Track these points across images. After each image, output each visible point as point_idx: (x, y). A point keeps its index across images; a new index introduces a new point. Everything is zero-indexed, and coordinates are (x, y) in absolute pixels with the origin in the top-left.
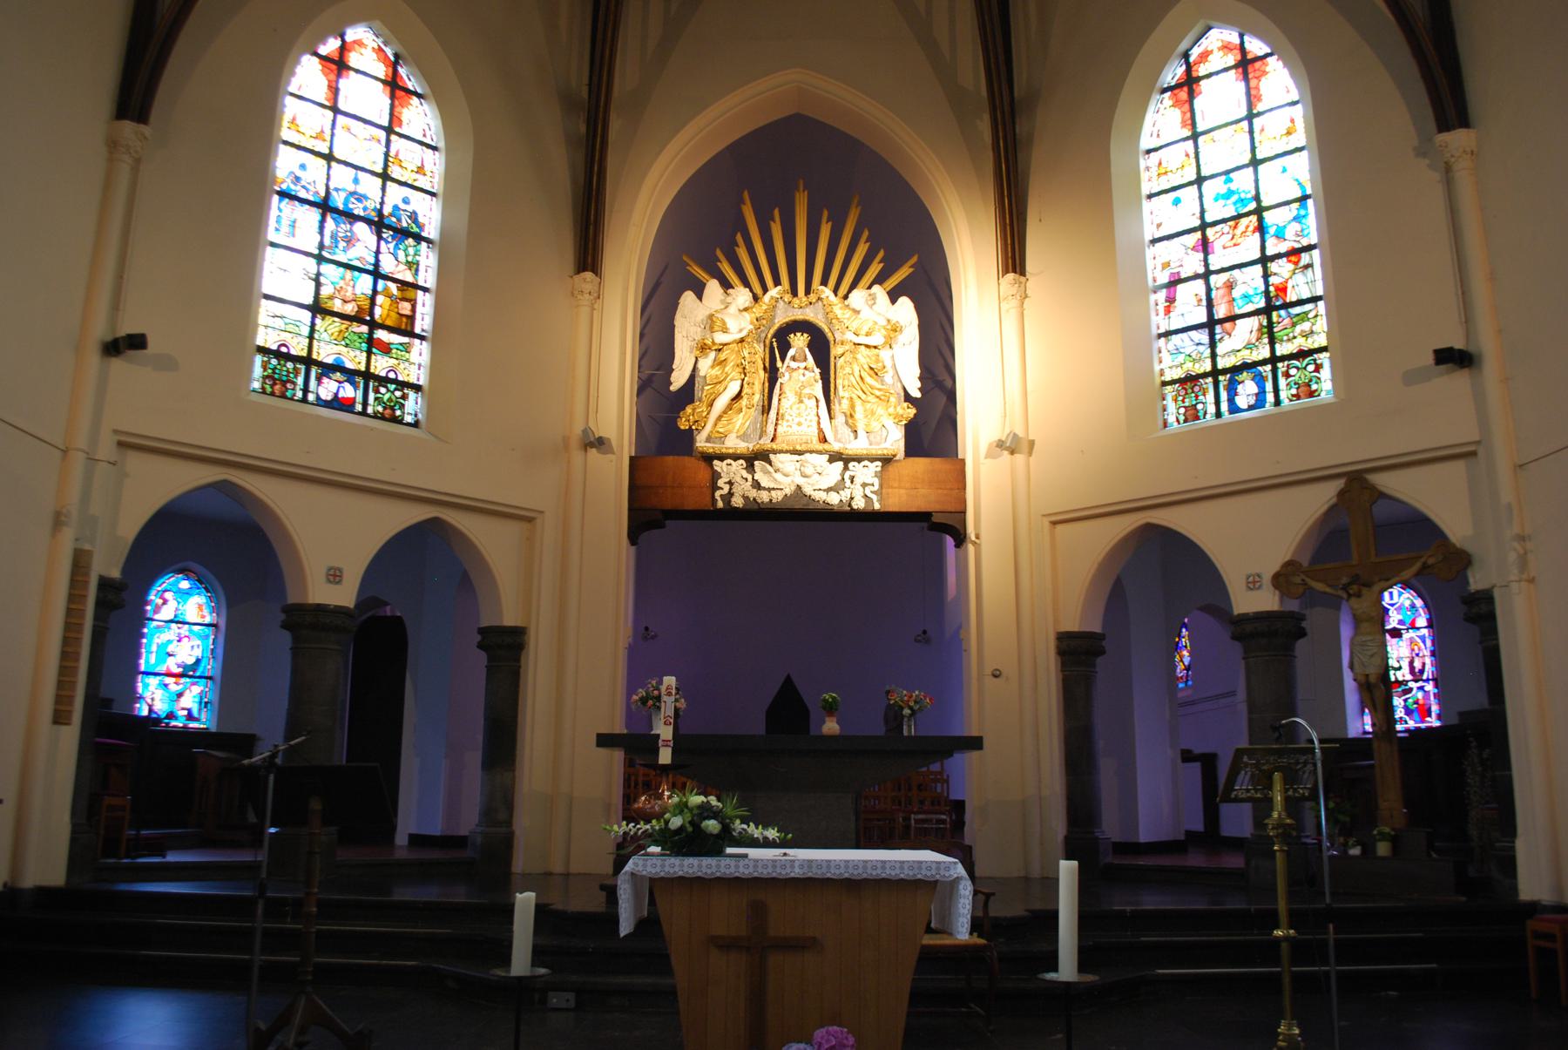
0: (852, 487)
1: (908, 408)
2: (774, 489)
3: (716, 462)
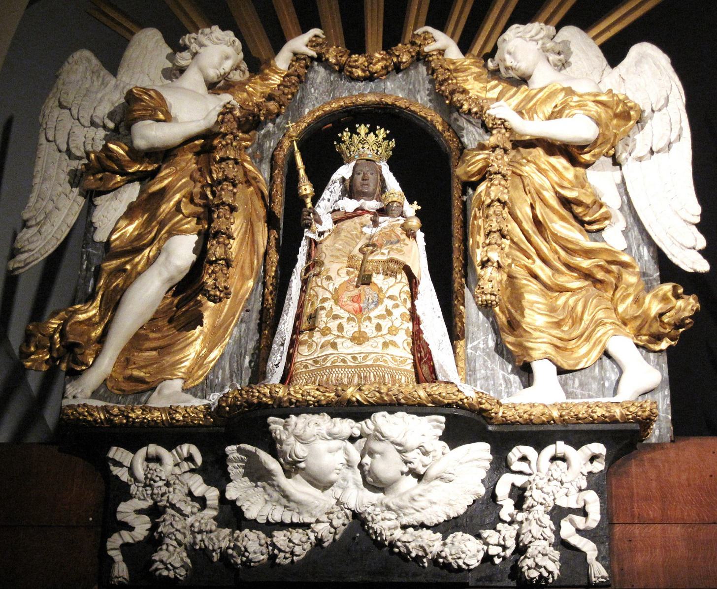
0: (520, 517)
1: (677, 297)
2: (282, 526)
3: (117, 453)
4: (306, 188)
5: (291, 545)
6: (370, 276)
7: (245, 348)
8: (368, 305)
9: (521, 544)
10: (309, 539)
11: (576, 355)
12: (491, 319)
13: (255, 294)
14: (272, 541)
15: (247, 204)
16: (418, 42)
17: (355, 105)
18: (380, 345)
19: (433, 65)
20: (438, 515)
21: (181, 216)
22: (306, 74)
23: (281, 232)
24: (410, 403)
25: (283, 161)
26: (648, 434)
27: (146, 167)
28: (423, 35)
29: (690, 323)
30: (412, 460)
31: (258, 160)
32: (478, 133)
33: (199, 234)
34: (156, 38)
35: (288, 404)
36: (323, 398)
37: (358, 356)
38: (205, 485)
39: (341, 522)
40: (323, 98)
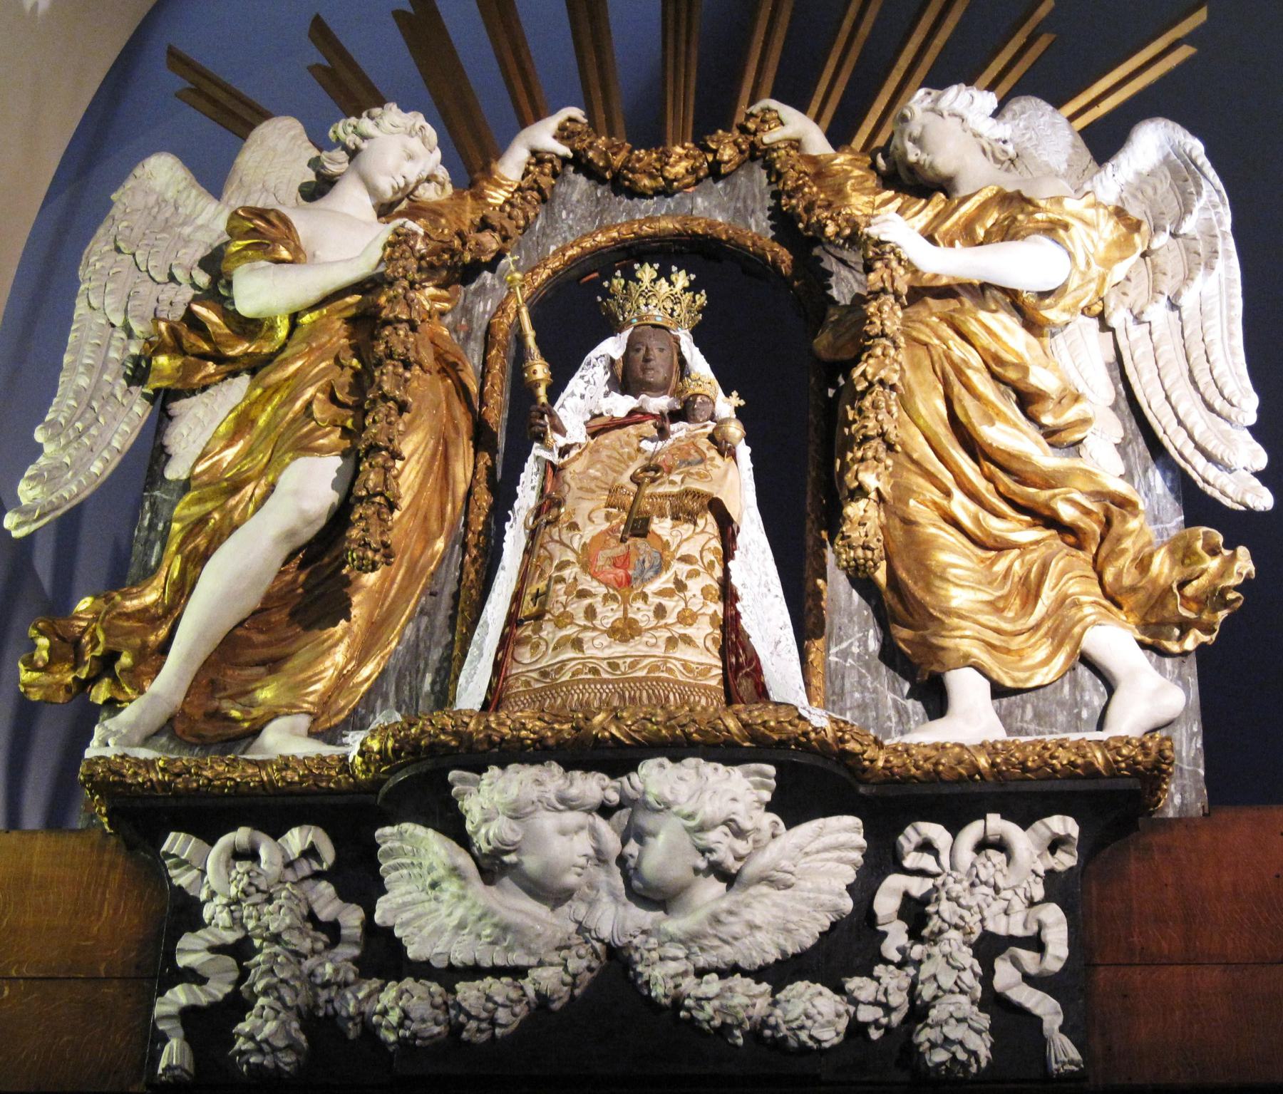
0: (917, 951)
3: (176, 842)
4: (540, 370)
5: (490, 1005)
6: (647, 521)
7: (426, 660)
8: (642, 572)
9: (919, 1002)
10: (524, 995)
11: (1028, 662)
12: (874, 602)
13: (448, 566)
14: (455, 1000)
15: (437, 407)
16: (751, 126)
17: (639, 237)
18: (662, 644)
19: (778, 166)
20: (766, 948)
21: (313, 423)
22: (553, 186)
23: (499, 458)
24: (711, 740)
25: (506, 335)
26: (1159, 800)
27: (261, 347)
28: (761, 114)
29: (1237, 599)
30: (713, 846)
31: (462, 335)
32: (856, 280)
33: (344, 455)
34: (292, 133)
35: (486, 746)
36: (549, 734)
37: (620, 662)
38: (338, 902)
39: (584, 963)
40: (582, 228)
